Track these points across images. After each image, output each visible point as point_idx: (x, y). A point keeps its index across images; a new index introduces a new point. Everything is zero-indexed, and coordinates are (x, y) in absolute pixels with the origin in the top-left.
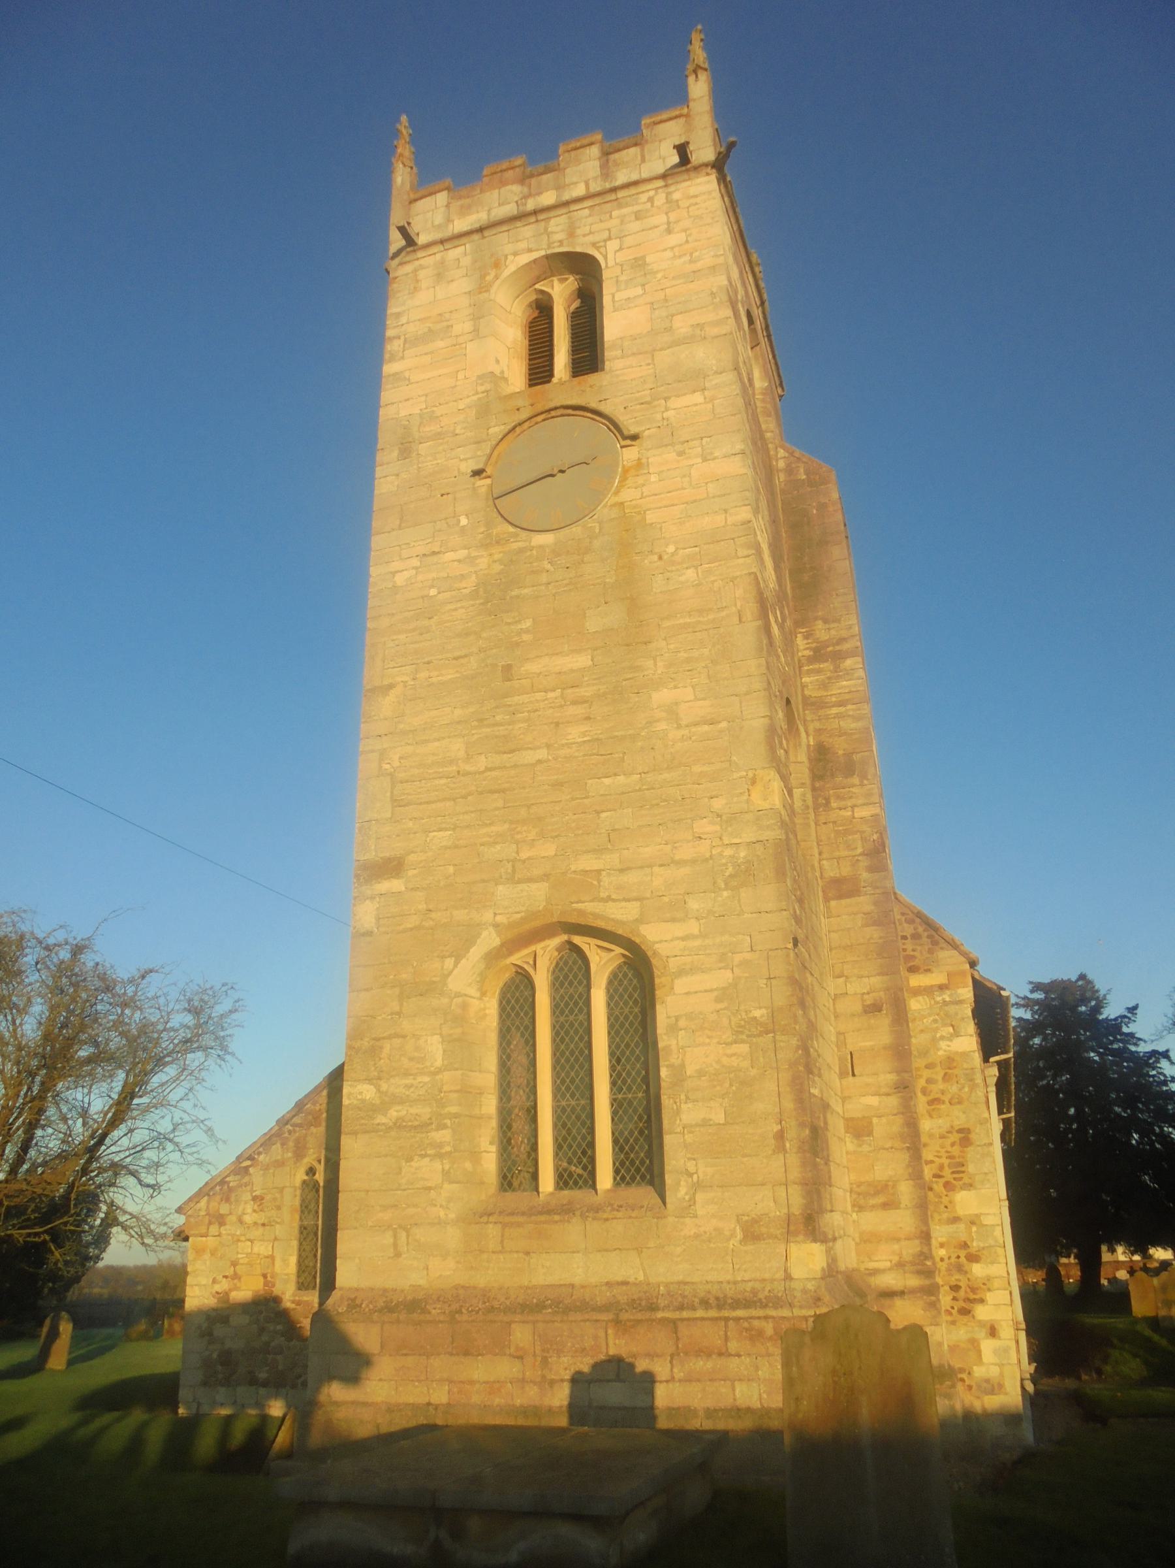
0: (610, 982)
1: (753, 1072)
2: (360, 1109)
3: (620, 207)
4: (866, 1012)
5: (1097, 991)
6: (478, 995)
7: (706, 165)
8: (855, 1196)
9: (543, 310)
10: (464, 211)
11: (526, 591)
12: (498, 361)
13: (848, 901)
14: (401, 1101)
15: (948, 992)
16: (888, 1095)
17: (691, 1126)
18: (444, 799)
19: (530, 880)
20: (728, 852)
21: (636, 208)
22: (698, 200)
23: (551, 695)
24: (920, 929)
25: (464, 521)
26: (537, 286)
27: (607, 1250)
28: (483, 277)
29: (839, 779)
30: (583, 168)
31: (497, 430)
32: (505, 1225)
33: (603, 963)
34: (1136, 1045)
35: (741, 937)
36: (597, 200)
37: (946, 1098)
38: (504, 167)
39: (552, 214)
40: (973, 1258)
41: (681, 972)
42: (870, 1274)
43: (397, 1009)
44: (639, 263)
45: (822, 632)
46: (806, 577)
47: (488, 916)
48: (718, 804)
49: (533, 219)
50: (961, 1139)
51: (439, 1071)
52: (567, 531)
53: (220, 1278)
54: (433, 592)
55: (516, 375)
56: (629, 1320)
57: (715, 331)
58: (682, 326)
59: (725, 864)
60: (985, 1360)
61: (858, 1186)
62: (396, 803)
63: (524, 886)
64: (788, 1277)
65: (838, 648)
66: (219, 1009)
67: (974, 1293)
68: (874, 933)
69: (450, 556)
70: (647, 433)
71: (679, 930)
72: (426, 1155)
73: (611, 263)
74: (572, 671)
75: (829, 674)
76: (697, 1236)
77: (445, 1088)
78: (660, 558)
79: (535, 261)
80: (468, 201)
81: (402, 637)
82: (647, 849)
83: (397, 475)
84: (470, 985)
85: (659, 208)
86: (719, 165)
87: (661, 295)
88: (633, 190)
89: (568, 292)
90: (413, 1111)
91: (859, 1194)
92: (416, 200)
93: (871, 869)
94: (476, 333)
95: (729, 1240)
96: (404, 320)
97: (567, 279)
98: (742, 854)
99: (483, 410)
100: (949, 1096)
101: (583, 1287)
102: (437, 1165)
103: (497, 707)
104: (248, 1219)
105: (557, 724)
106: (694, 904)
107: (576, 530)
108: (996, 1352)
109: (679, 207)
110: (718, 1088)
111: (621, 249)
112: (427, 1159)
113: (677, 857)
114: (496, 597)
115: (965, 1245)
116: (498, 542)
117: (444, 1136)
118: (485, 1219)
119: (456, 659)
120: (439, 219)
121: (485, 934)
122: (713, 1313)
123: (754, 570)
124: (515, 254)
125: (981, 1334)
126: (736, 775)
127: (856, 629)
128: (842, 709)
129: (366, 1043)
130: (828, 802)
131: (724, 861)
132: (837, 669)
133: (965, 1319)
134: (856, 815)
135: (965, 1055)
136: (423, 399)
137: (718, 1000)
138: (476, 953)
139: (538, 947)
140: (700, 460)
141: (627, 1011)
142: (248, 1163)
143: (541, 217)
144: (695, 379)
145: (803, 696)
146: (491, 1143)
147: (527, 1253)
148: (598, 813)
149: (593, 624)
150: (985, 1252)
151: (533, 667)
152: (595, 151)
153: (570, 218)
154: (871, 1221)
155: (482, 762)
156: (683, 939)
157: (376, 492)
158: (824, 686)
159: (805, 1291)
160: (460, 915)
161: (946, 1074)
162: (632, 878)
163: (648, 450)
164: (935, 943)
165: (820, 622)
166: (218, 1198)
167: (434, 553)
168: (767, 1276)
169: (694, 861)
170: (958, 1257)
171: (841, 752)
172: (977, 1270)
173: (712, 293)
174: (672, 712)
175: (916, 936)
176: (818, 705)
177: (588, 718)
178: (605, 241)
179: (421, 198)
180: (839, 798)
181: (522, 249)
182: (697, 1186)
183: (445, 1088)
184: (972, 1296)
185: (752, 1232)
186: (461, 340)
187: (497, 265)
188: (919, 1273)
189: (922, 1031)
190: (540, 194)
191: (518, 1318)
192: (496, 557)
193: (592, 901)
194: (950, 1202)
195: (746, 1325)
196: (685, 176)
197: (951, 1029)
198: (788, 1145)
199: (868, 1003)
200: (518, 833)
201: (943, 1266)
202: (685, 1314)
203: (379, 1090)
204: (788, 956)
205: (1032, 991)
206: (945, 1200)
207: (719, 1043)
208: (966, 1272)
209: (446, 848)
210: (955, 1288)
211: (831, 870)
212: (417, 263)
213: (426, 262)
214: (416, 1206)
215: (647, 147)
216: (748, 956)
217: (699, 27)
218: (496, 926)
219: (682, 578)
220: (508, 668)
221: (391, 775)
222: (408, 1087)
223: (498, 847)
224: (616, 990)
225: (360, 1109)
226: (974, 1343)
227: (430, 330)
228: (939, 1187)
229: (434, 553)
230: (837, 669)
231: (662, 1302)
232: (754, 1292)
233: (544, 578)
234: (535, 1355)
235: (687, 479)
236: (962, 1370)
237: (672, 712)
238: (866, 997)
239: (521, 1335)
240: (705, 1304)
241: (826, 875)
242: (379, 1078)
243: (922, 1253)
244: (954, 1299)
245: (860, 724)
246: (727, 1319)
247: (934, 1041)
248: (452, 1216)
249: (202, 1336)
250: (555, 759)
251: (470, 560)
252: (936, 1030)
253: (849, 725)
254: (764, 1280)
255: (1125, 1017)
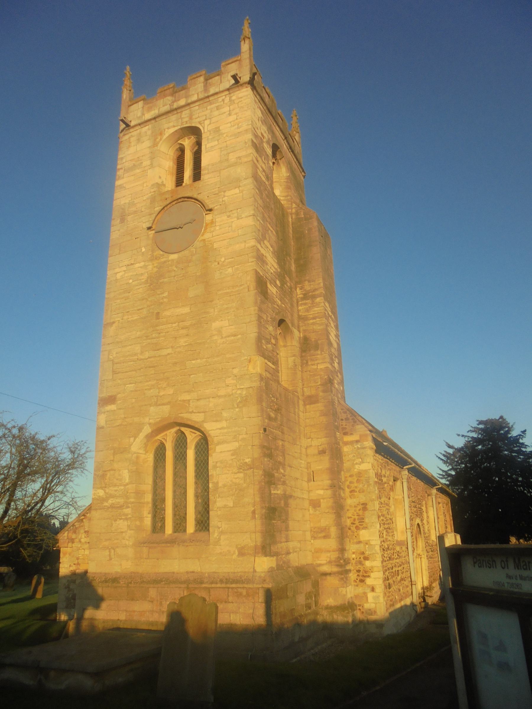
0: (196, 447)
1: (245, 485)
2: (98, 500)
3: (211, 104)
4: (319, 454)
5: (509, 424)
6: (144, 452)
7: (245, 83)
8: (312, 533)
9: (182, 150)
10: (150, 109)
11: (165, 280)
12: (160, 177)
13: (314, 405)
15: (360, 444)
16: (327, 489)
17: (220, 508)
18: (132, 371)
19: (163, 404)
20: (239, 392)
21: (217, 105)
22: (242, 99)
23: (174, 325)
24: (349, 416)
25: (143, 250)
26: (179, 142)
27: (187, 559)
28: (155, 140)
29: (312, 352)
30: (197, 88)
31: (158, 209)
32: (150, 548)
33: (192, 438)
34: (525, 448)
35: (242, 428)
36: (202, 102)
37: (357, 490)
38: (166, 88)
39: (183, 109)
40: (366, 559)
41: (219, 443)
42: (318, 566)
43: (112, 459)
44: (217, 130)
45: (308, 286)
46: (302, 262)
47: (147, 420)
48: (235, 371)
49: (175, 112)
50: (363, 508)
51: (127, 484)
52: (183, 253)
53: (72, 565)
54: (131, 281)
55: (170, 183)
56: (192, 588)
57: (246, 160)
58: (232, 158)
59: (237, 397)
60: (369, 601)
61: (314, 529)
62: (114, 372)
63: (161, 407)
64: (255, 571)
65: (314, 293)
66: (83, 451)
67: (366, 573)
68: (324, 419)
69: (138, 265)
70: (216, 208)
71: (218, 425)
72: (122, 519)
73: (206, 130)
74: (182, 314)
75: (310, 305)
76: (221, 553)
77: (129, 491)
78: (218, 263)
79: (176, 131)
80: (151, 105)
81: (119, 301)
82: (207, 391)
84: (140, 449)
85: (226, 104)
86: (251, 82)
87: (225, 144)
88: (216, 97)
89: (191, 144)
90: (118, 500)
91: (314, 532)
92: (131, 105)
93: (324, 391)
94: (152, 166)
95: (233, 555)
96: (124, 161)
97: (190, 138)
98: (244, 393)
99: (153, 200)
100: (359, 489)
101: (177, 573)
102: (126, 523)
103: (153, 331)
104: (83, 540)
105: (176, 338)
106: (225, 414)
107: (186, 252)
108: (374, 598)
109: (234, 103)
110: (231, 492)
111: (210, 124)
112: (122, 520)
113: (219, 394)
114: (154, 282)
115: (363, 553)
116: (156, 259)
117: (128, 511)
118: (142, 545)
119: (138, 310)
120: (139, 114)
121: (145, 427)
122: (223, 585)
123: (255, 268)
124: (168, 128)
125: (368, 590)
126: (243, 359)
127: (322, 284)
128: (314, 321)
129: (101, 473)
130: (307, 362)
131: (237, 396)
132: (313, 302)
133: (362, 584)
134: (318, 367)
135: (366, 471)
136: (130, 196)
137: (232, 455)
138: (142, 435)
139: (168, 432)
140: (236, 219)
141: (202, 458)
142: (83, 517)
143: (179, 111)
144: (235, 182)
145: (298, 315)
146: (149, 513)
147: (158, 559)
148: (190, 375)
149: (191, 293)
150: (371, 556)
151: (167, 313)
152: (202, 79)
153: (190, 111)
154: (319, 543)
155: (147, 355)
156: (220, 429)
157: (111, 238)
158: (307, 310)
159: (260, 577)
160: (136, 419)
161: (358, 480)
162: (202, 403)
163: (216, 215)
164: (355, 422)
165: (307, 282)
166: (72, 531)
167: (132, 264)
168: (246, 570)
169: (225, 396)
170: (360, 558)
171: (313, 340)
172: (368, 563)
173: (246, 142)
174: (219, 331)
175: (347, 419)
176: (304, 319)
177: (187, 335)
178: (204, 121)
179: (133, 104)
180: (312, 360)
181: (171, 126)
182: (222, 533)
183: (129, 491)
184: (365, 575)
185: (242, 553)
186: (146, 168)
187: (161, 134)
188: (337, 566)
189: (348, 461)
190: (179, 100)
191: (152, 585)
192: (155, 265)
193: (186, 413)
194: (358, 535)
195: (236, 590)
196: (237, 89)
197: (360, 460)
198: (257, 516)
199: (320, 449)
200: (160, 384)
201: (354, 562)
202: (213, 586)
203: (105, 492)
204: (260, 436)
205: (478, 425)
206: (356, 534)
207: (232, 473)
208: (363, 565)
209: (132, 391)
210: (359, 571)
211: (307, 392)
212: (130, 134)
213: (134, 133)
214: (117, 539)
215: (223, 76)
216: (245, 436)
217: (247, 18)
218: (150, 424)
219: (227, 272)
220: (158, 313)
221: (112, 360)
222: (116, 491)
223: (152, 391)
224: (198, 450)
225: (98, 500)
226: (365, 594)
227: (134, 165)
228: (353, 528)
229: (132, 264)
230: (313, 302)
231: (206, 580)
232: (241, 577)
233: (173, 274)
234: (157, 601)
235: (230, 228)
236: (360, 605)
237: (219, 331)
238: (319, 447)
239: (153, 593)
240: (221, 581)
241: (305, 394)
242: (106, 487)
243: (339, 557)
244: (358, 575)
245: (322, 327)
246: (228, 588)
247: (353, 465)
248: (131, 543)
249: (66, 588)
250: (175, 353)
251: (145, 267)
252: (354, 460)
253: (317, 328)
254: (245, 572)
255: (521, 435)
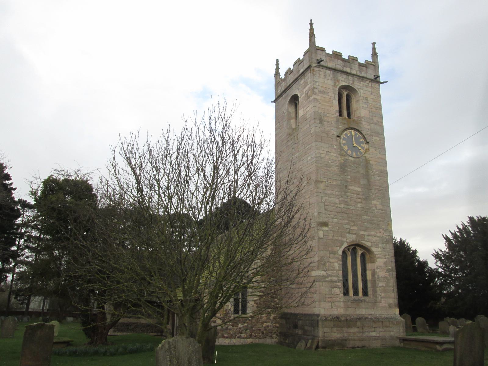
14: (331, 276)
18: (335, 212)
21: (366, 84)
25: (335, 147)
41: (379, 258)
43: (329, 256)
44: (366, 98)
48: (383, 226)
54: (330, 162)
69: (332, 154)
83: (320, 128)
106: (380, 245)
111: (363, 93)
119: (336, 180)
121: (345, 243)
137: (384, 264)
155: (342, 206)
160: (340, 238)
162: (370, 238)
174: (375, 205)
182: (381, 298)
216: (388, 257)
218: (347, 242)
222: (332, 273)
